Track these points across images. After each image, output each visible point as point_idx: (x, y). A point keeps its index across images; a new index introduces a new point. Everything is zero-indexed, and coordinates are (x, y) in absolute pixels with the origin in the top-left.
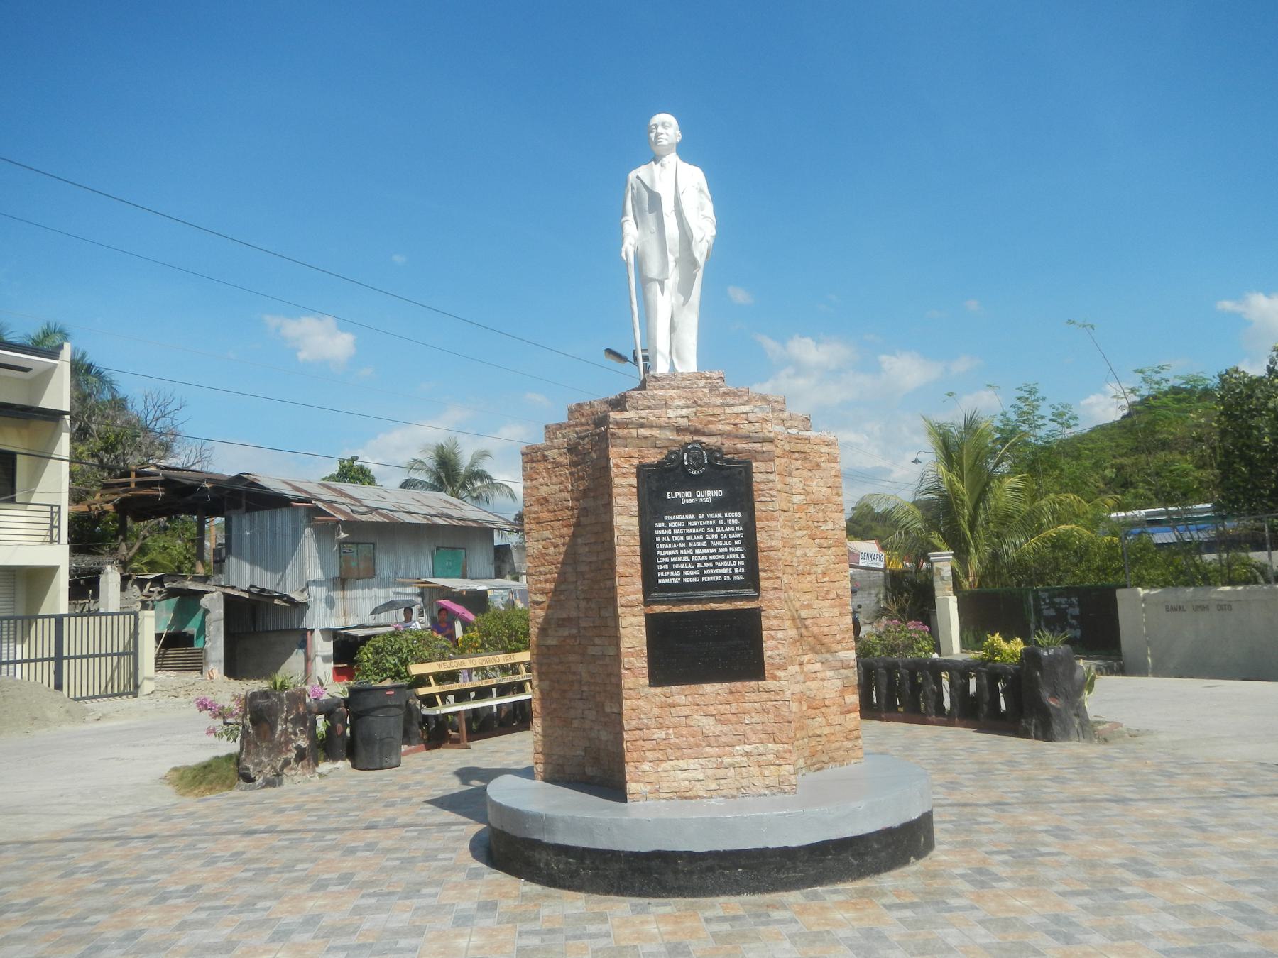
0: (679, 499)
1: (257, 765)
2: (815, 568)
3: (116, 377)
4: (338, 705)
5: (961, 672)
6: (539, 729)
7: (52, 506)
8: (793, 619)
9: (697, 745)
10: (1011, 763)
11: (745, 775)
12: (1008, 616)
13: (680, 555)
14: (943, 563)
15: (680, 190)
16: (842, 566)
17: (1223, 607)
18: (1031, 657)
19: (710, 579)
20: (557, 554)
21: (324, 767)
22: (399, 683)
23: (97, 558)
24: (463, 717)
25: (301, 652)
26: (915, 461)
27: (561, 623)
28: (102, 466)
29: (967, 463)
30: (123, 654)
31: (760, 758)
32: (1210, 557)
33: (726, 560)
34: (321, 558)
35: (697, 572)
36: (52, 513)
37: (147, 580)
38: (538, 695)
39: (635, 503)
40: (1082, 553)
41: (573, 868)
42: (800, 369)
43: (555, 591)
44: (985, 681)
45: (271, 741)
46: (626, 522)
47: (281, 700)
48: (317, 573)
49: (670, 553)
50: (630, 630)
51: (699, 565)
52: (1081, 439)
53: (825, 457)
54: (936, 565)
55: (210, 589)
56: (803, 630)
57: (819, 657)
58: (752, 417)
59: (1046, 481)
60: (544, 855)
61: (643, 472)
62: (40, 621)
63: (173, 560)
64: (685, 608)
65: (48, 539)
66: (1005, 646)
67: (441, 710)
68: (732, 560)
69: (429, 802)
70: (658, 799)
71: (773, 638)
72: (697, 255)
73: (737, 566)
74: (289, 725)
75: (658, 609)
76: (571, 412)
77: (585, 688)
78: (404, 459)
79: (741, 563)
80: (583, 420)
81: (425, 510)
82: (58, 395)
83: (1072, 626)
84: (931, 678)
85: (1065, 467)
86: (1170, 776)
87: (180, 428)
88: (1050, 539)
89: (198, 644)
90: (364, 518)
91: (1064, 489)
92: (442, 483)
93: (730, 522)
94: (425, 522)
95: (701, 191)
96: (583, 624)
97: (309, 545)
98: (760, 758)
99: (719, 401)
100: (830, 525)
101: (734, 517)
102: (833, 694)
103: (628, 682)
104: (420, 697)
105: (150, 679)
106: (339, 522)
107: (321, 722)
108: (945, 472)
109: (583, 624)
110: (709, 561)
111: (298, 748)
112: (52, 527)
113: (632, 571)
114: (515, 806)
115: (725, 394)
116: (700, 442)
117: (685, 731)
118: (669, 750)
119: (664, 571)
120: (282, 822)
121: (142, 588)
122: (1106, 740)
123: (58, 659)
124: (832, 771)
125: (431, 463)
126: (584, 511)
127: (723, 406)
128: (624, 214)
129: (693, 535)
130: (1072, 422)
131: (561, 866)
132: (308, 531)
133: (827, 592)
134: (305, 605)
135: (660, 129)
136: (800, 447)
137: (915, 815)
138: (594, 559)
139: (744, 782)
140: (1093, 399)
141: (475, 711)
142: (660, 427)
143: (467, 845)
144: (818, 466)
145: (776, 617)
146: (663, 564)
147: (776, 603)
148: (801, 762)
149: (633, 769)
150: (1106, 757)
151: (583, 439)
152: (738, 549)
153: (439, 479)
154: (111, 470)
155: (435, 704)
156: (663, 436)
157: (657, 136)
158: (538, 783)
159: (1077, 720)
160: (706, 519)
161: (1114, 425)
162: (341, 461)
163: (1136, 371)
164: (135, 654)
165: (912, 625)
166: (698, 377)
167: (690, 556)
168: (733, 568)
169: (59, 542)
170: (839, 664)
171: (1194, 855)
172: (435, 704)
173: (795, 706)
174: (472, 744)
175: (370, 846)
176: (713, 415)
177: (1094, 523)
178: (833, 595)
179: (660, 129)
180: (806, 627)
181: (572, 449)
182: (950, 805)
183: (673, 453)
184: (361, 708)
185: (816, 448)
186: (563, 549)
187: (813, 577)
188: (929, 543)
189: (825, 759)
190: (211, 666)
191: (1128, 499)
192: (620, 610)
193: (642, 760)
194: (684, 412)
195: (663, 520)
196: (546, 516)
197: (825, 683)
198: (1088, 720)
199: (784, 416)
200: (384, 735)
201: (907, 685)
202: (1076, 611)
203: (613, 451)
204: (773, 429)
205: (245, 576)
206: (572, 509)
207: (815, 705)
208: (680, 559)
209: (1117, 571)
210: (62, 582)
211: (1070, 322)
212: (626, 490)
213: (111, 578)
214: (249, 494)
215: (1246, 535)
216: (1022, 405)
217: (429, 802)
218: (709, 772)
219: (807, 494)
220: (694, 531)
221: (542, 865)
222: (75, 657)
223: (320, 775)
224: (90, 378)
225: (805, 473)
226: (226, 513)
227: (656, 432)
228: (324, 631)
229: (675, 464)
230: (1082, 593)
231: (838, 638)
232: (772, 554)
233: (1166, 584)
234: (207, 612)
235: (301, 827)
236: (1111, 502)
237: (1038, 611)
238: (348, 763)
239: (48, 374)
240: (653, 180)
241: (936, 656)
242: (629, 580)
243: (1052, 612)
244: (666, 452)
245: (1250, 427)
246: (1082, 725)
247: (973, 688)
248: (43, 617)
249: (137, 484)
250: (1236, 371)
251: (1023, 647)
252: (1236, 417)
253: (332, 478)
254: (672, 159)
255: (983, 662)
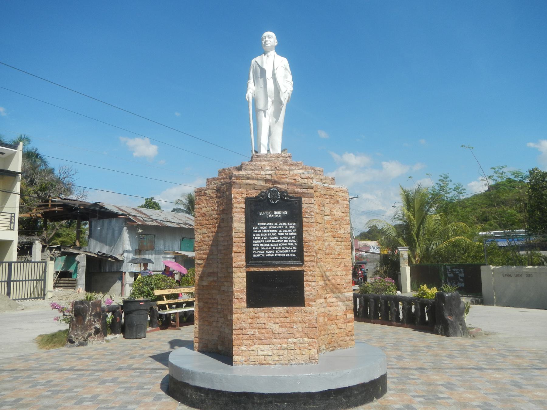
0: (265, 215)
1: (76, 335)
2: (334, 252)
3: (48, 160)
4: (118, 308)
5: (408, 302)
6: (197, 326)
7: (11, 214)
8: (322, 276)
9: (270, 338)
10: (429, 347)
11: (292, 354)
12: (432, 276)
13: (265, 243)
14: (404, 252)
15: (275, 68)
16: (348, 251)
17: (529, 275)
18: (440, 297)
19: (279, 255)
20: (209, 241)
21: (110, 337)
22: (149, 299)
23: (31, 238)
24: (178, 315)
25: (120, 282)
26: (393, 206)
27: (210, 274)
28: (39, 197)
29: (416, 207)
30: (39, 280)
31: (300, 345)
32: (522, 253)
33: (287, 246)
34: (130, 241)
35: (273, 252)
36: (11, 217)
37: (53, 248)
38: (197, 309)
39: (243, 216)
40: (466, 250)
41: (203, 398)
42: (348, 167)
43: (207, 259)
44: (419, 307)
45: (83, 324)
46: (239, 226)
47: (89, 305)
48: (128, 247)
49: (260, 242)
50: (238, 279)
51: (274, 248)
52: (467, 200)
53: (341, 198)
54: (401, 252)
55: (80, 252)
56: (327, 282)
57: (334, 295)
58: (303, 176)
59: (451, 217)
60: (190, 391)
61: (249, 201)
62: (4, 264)
63: (72, 239)
64: (266, 269)
65: (9, 228)
66: (428, 291)
67: (168, 311)
68: (290, 246)
69: (151, 357)
70: (249, 364)
71: (309, 285)
72: (282, 99)
73: (293, 249)
74: (92, 317)
75: (253, 269)
76: (220, 173)
77: (219, 307)
78: (175, 200)
79: (295, 248)
80: (225, 176)
81: (178, 221)
82: (17, 165)
83: (460, 282)
84: (394, 305)
85: (460, 211)
86: (504, 356)
87: (74, 182)
88: (452, 242)
89: (74, 277)
90: (150, 224)
91: (459, 220)
92: (190, 210)
93: (290, 227)
94: (177, 226)
95: (286, 69)
96: (220, 275)
97: (125, 235)
98: (300, 345)
99: (287, 168)
100: (342, 231)
101: (292, 225)
102: (341, 314)
103: (236, 305)
104: (158, 306)
105: (51, 292)
106: (138, 225)
107: (110, 315)
108: (406, 211)
109: (220, 275)
110: (279, 246)
111: (96, 328)
112: (11, 223)
113: (241, 250)
114: (178, 365)
115: (291, 164)
116: (277, 188)
117: (263, 331)
118: (255, 340)
119: (256, 250)
120: (78, 365)
121: (51, 251)
122: (474, 336)
123: (9, 281)
124: (339, 351)
125: (185, 201)
126: (222, 220)
127: (289, 170)
128: (249, 79)
129: (271, 233)
130: (463, 191)
131: (197, 397)
132: (125, 228)
133: (340, 263)
134: (122, 261)
135: (267, 39)
136: (329, 192)
137: (377, 377)
138: (226, 244)
139: (292, 357)
140: (473, 183)
141: (185, 313)
142: (257, 179)
143: (160, 381)
144: (338, 202)
145: (311, 275)
146: (256, 247)
147: (312, 268)
148: (323, 347)
149: (237, 349)
150: (473, 345)
151: (223, 185)
152: (293, 241)
153: (189, 208)
154: (42, 199)
155: (166, 309)
156: (259, 184)
157: (265, 42)
158: (195, 352)
159: (461, 327)
160: (278, 225)
161: (482, 195)
162: (146, 199)
163: (492, 168)
164: (45, 280)
165: (387, 279)
166: (279, 156)
167: (269, 243)
168: (291, 250)
169: (14, 230)
170: (345, 299)
171: (516, 402)
172: (166, 309)
173: (321, 319)
174: (182, 328)
175: (114, 380)
176: (284, 175)
177: (472, 236)
178: (343, 265)
179: (267, 39)
180: (329, 280)
181: (218, 190)
182: (397, 368)
183: (263, 192)
184: (128, 310)
185: (337, 193)
186: (212, 238)
187: (333, 256)
188: (399, 243)
189: (336, 345)
190: (79, 287)
191: (487, 226)
192: (234, 269)
193: (241, 345)
194: (269, 172)
195: (257, 225)
196: (205, 222)
197: (337, 308)
198: (466, 327)
199: (322, 177)
200: (138, 323)
201: (383, 307)
202: (462, 275)
203: (234, 191)
204: (314, 182)
205: (97, 247)
206: (217, 219)
207: (332, 318)
208: (265, 245)
209: (481, 257)
210: (15, 247)
211: (462, 146)
212: (239, 210)
213: (37, 246)
214: (100, 212)
215: (538, 244)
216: (441, 183)
217: (151, 357)
218: (275, 352)
219: (332, 215)
220: (272, 231)
221: (188, 396)
222: (17, 281)
223: (107, 341)
224: (37, 159)
225: (331, 205)
226: (90, 220)
227: (255, 182)
228: (130, 273)
229: (264, 198)
230: (465, 267)
231: (345, 286)
232: (311, 244)
233: (503, 264)
234: (78, 262)
235: (86, 368)
236: (480, 227)
237: (446, 275)
238: (122, 335)
239: (12, 156)
240: (262, 63)
241: (399, 292)
242: (239, 254)
243: (452, 275)
244: (260, 192)
245: (543, 195)
246: (463, 329)
247: (413, 310)
248: (6, 262)
249: (52, 205)
250: (536, 169)
251: (437, 291)
252: (537, 190)
253: (142, 206)
254: (272, 53)
255: (418, 298)
